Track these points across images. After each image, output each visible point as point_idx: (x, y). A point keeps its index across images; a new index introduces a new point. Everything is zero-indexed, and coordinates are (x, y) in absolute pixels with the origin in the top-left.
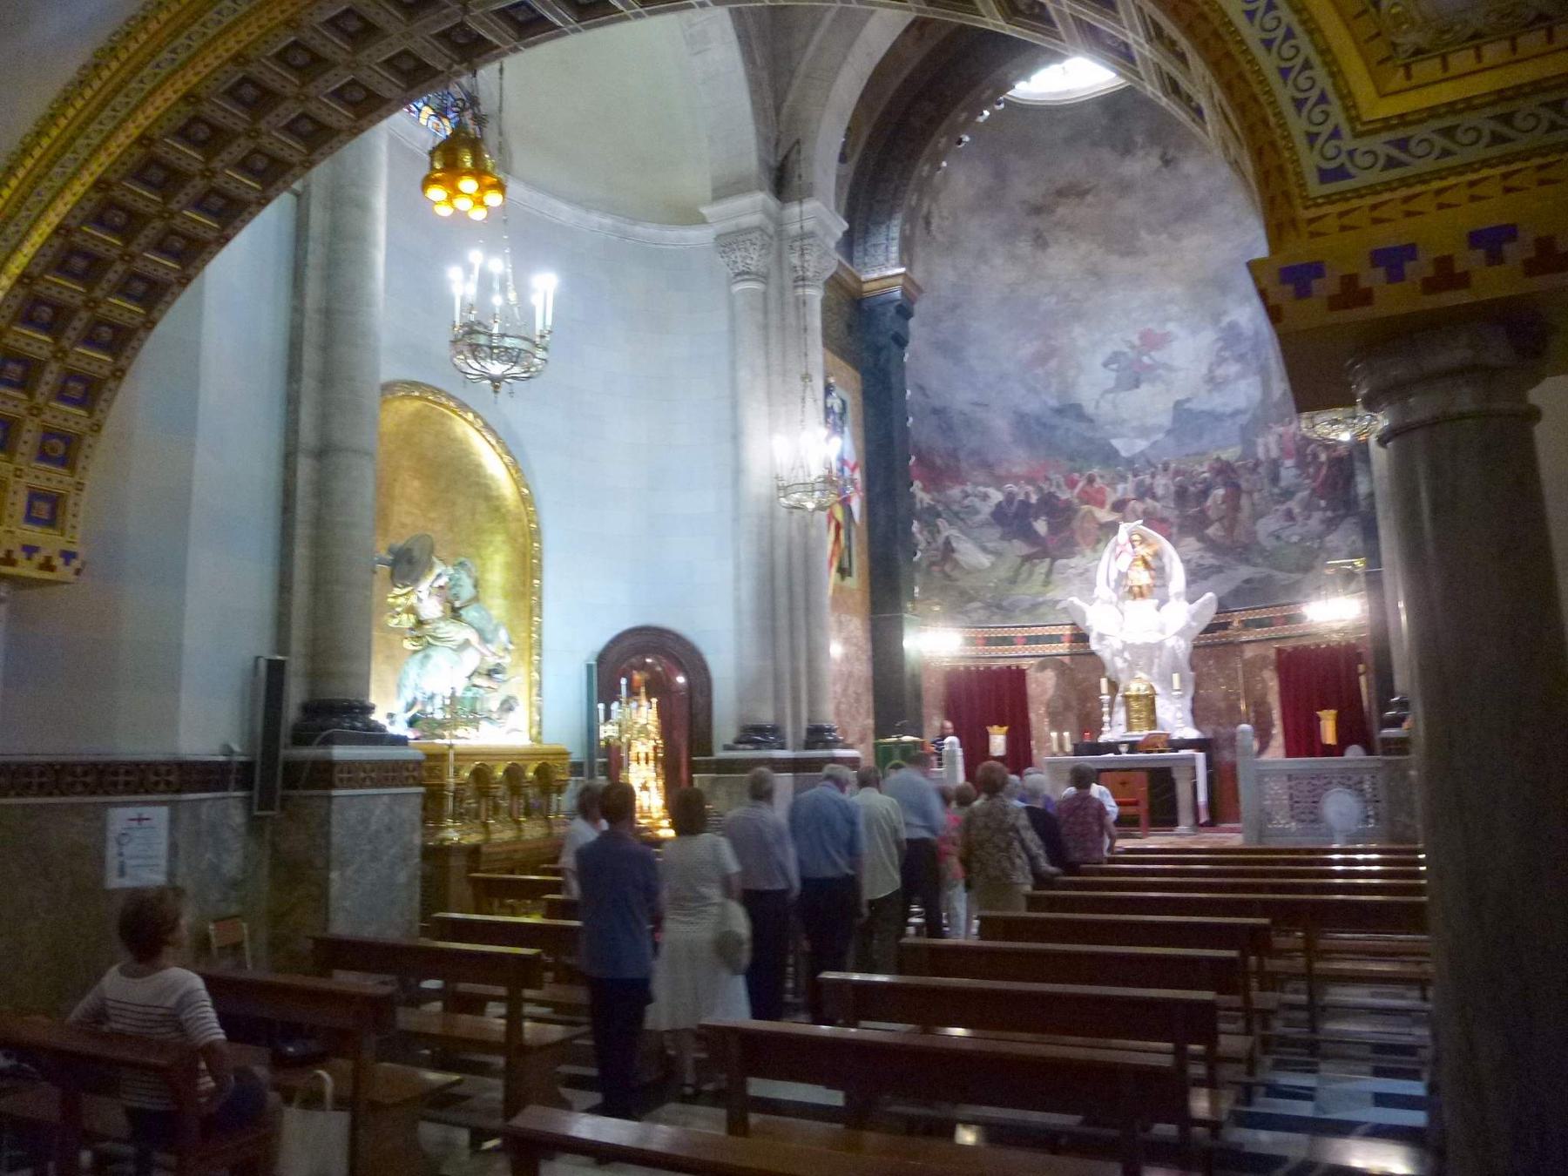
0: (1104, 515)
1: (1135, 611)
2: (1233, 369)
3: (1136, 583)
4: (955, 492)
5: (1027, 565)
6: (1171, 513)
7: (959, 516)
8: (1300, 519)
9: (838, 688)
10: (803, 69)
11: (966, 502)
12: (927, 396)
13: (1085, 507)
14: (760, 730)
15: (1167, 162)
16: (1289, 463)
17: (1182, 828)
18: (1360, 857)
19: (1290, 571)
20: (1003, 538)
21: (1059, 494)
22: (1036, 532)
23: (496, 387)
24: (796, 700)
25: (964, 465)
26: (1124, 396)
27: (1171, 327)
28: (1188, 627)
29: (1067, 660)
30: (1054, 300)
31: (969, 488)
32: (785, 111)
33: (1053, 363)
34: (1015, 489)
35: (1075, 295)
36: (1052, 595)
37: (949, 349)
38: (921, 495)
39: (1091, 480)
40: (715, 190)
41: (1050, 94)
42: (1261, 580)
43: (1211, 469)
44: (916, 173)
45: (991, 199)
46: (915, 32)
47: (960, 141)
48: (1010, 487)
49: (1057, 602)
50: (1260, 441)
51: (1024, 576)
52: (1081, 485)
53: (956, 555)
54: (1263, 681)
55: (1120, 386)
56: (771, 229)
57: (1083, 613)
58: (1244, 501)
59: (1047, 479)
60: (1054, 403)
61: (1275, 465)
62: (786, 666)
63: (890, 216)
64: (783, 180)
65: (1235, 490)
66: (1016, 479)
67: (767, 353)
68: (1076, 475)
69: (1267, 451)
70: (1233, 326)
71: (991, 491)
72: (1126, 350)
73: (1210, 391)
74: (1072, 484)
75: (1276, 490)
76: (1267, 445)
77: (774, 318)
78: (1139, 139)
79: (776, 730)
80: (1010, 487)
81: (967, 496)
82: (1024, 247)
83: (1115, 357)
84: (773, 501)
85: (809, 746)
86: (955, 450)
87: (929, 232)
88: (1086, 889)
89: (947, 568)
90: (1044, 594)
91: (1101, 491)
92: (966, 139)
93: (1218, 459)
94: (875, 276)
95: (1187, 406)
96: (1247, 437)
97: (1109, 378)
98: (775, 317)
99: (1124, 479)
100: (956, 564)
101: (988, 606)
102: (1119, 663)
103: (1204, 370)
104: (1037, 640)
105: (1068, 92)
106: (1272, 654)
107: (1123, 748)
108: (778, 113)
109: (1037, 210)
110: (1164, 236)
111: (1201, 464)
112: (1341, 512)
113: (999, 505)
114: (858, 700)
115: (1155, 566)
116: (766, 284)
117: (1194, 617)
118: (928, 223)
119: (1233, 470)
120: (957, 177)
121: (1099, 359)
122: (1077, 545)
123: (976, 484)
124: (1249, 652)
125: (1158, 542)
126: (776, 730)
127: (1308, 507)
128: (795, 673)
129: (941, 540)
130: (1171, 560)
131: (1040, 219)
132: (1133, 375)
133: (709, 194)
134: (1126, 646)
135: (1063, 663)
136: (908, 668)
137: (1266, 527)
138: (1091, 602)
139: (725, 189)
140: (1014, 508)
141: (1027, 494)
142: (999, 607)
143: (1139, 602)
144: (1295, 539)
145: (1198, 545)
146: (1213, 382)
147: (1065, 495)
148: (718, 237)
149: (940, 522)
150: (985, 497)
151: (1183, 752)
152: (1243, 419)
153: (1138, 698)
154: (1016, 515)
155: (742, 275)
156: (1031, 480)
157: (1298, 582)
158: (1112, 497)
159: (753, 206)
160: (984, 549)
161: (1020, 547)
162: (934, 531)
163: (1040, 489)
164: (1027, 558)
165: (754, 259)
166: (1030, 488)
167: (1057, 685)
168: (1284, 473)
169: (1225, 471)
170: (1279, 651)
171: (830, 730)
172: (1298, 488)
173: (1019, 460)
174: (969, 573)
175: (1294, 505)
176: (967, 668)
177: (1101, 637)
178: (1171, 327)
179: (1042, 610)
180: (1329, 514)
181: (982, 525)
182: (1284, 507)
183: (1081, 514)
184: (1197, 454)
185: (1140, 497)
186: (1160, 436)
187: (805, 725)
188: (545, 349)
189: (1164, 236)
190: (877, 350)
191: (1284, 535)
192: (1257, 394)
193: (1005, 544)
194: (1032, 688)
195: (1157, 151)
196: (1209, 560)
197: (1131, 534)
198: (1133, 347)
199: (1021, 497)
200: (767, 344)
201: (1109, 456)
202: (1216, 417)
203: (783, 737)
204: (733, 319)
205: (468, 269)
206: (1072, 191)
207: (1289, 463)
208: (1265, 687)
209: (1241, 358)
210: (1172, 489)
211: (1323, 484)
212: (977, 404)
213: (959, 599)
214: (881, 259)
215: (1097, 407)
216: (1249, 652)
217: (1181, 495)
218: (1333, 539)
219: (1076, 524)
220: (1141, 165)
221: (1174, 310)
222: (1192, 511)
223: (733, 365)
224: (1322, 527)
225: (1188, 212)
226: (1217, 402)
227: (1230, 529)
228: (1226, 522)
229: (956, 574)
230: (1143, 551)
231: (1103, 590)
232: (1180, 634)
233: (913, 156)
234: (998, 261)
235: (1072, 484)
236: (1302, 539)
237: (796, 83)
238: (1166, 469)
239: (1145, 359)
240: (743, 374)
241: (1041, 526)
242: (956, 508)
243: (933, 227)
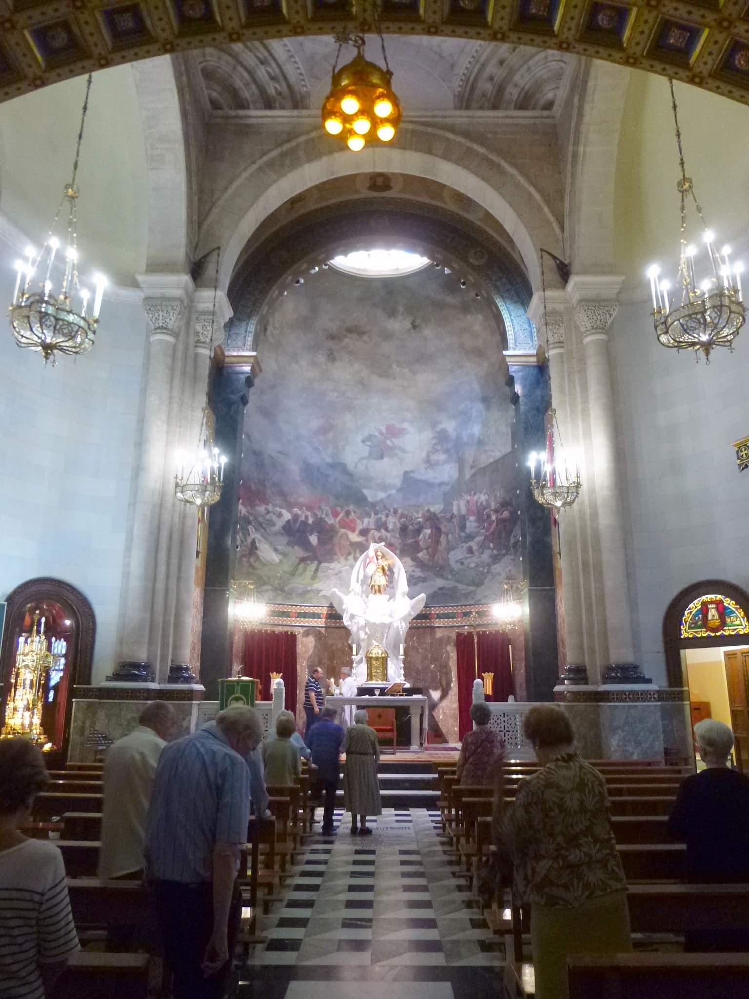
0: (354, 537)
1: (375, 601)
2: (442, 457)
3: (378, 583)
4: (261, 509)
5: (302, 565)
6: (397, 541)
7: (263, 526)
8: (477, 554)
10: (221, 203)
11: (268, 517)
12: (251, 442)
13: (343, 530)
14: (136, 666)
15: (414, 327)
16: (472, 518)
17: (415, 747)
18: (519, 768)
19: (468, 585)
20: (288, 544)
21: (327, 520)
22: (309, 543)
23: (47, 354)
24: (165, 645)
25: (269, 492)
26: (375, 462)
27: (405, 425)
28: (410, 615)
29: (323, 630)
30: (336, 394)
31: (270, 508)
32: (205, 226)
33: (330, 435)
34: (299, 512)
35: (349, 394)
36: (317, 586)
37: (267, 413)
38: (242, 509)
39: (348, 513)
40: (148, 265)
41: (358, 270)
42: (449, 589)
43: (423, 516)
44: (269, 296)
45: (305, 323)
46: (289, 204)
47: (298, 282)
48: (296, 510)
49: (319, 591)
50: (455, 503)
51: (300, 571)
52: (341, 516)
53: (258, 552)
54: (447, 652)
55: (370, 456)
56: (186, 303)
57: (341, 602)
58: (443, 539)
59: (320, 508)
60: (329, 460)
61: (463, 519)
62: (159, 619)
63: (249, 317)
64: (197, 271)
65: (437, 531)
66: (301, 506)
67: (171, 388)
68: (339, 509)
69: (459, 509)
70: (444, 432)
71: (284, 512)
72: (377, 434)
73: (426, 468)
74: (335, 514)
75: (463, 534)
76: (459, 506)
77: (179, 365)
78: (401, 309)
80: (296, 510)
81: (268, 512)
82: (321, 358)
83: (370, 437)
84: (163, 494)
85: (171, 680)
86: (264, 481)
87: (265, 335)
88: (659, 794)
89: (252, 560)
90: (311, 585)
91: (353, 521)
92: (302, 281)
93: (428, 511)
94: (235, 354)
95: (412, 475)
96: (447, 498)
97: (365, 450)
98: (181, 363)
99: (369, 516)
100: (258, 558)
101: (275, 589)
102: (362, 635)
103: (424, 455)
104: (305, 615)
105: (364, 270)
106: (454, 636)
107: (377, 692)
108: (200, 225)
109: (332, 337)
110: (407, 370)
111: (417, 512)
112: (504, 552)
113: (288, 522)
115: (388, 572)
116: (177, 340)
117: (413, 608)
119: (438, 519)
120: (288, 304)
121: (359, 438)
122: (336, 554)
123: (275, 506)
124: (439, 634)
125: (392, 558)
126: (147, 667)
127: (482, 547)
128: (166, 623)
129: (249, 540)
130: (399, 570)
131: (333, 343)
132: (380, 451)
133: (144, 268)
134: (367, 623)
135: (320, 632)
136: (229, 627)
137: (456, 555)
138: (347, 592)
139: (155, 267)
140: (297, 525)
141: (307, 517)
142: (282, 590)
143: (378, 596)
144: (473, 565)
145: (412, 563)
146: (429, 463)
147: (330, 521)
148: (147, 299)
149: (250, 527)
150: (280, 515)
151: (415, 696)
152: (446, 488)
153: (377, 659)
154: (298, 530)
155: (163, 329)
156: (309, 508)
157: (472, 592)
158: (360, 526)
159: (178, 282)
160: (276, 550)
161: (299, 552)
162: (246, 533)
163: (315, 515)
164: (303, 560)
165: (173, 320)
166: (309, 513)
167: (315, 647)
168: (468, 524)
169: (432, 519)
170: (459, 635)
171: (187, 669)
172: (477, 534)
173: (304, 494)
174: (265, 565)
175: (474, 545)
176: (260, 631)
177: (352, 617)
178: (405, 425)
179: (308, 596)
180: (495, 552)
181: (276, 534)
182: (468, 545)
183: (340, 534)
184: (415, 506)
185: (378, 529)
186: (393, 492)
188: (94, 332)
189: (407, 370)
190: (230, 404)
191: (466, 562)
192: (456, 475)
193: (290, 548)
194: (300, 648)
195: (411, 319)
196: (418, 573)
197: (376, 552)
198: (381, 433)
199: (303, 518)
200: (172, 382)
201: (360, 500)
202: (430, 485)
203: (153, 673)
204: (148, 356)
205: (26, 259)
206: (355, 330)
207: (472, 518)
208: (448, 657)
209: (447, 451)
210: (398, 525)
211: (493, 533)
212: (280, 452)
213: (262, 584)
214: (240, 344)
215: (356, 467)
216: (439, 634)
217: (404, 529)
218: (497, 568)
219: (336, 540)
220: (399, 325)
221: (409, 415)
222: (410, 541)
223: (144, 391)
224: (489, 560)
226: (430, 475)
227: (432, 556)
228: (430, 550)
229: (257, 565)
230: (384, 563)
231: (356, 586)
232: (404, 619)
233: (271, 281)
234: (303, 363)
235: (335, 514)
236: (477, 566)
237: (215, 211)
238: (395, 512)
239: (388, 442)
240: (153, 400)
241: (314, 539)
242: (261, 519)
243: (268, 332)
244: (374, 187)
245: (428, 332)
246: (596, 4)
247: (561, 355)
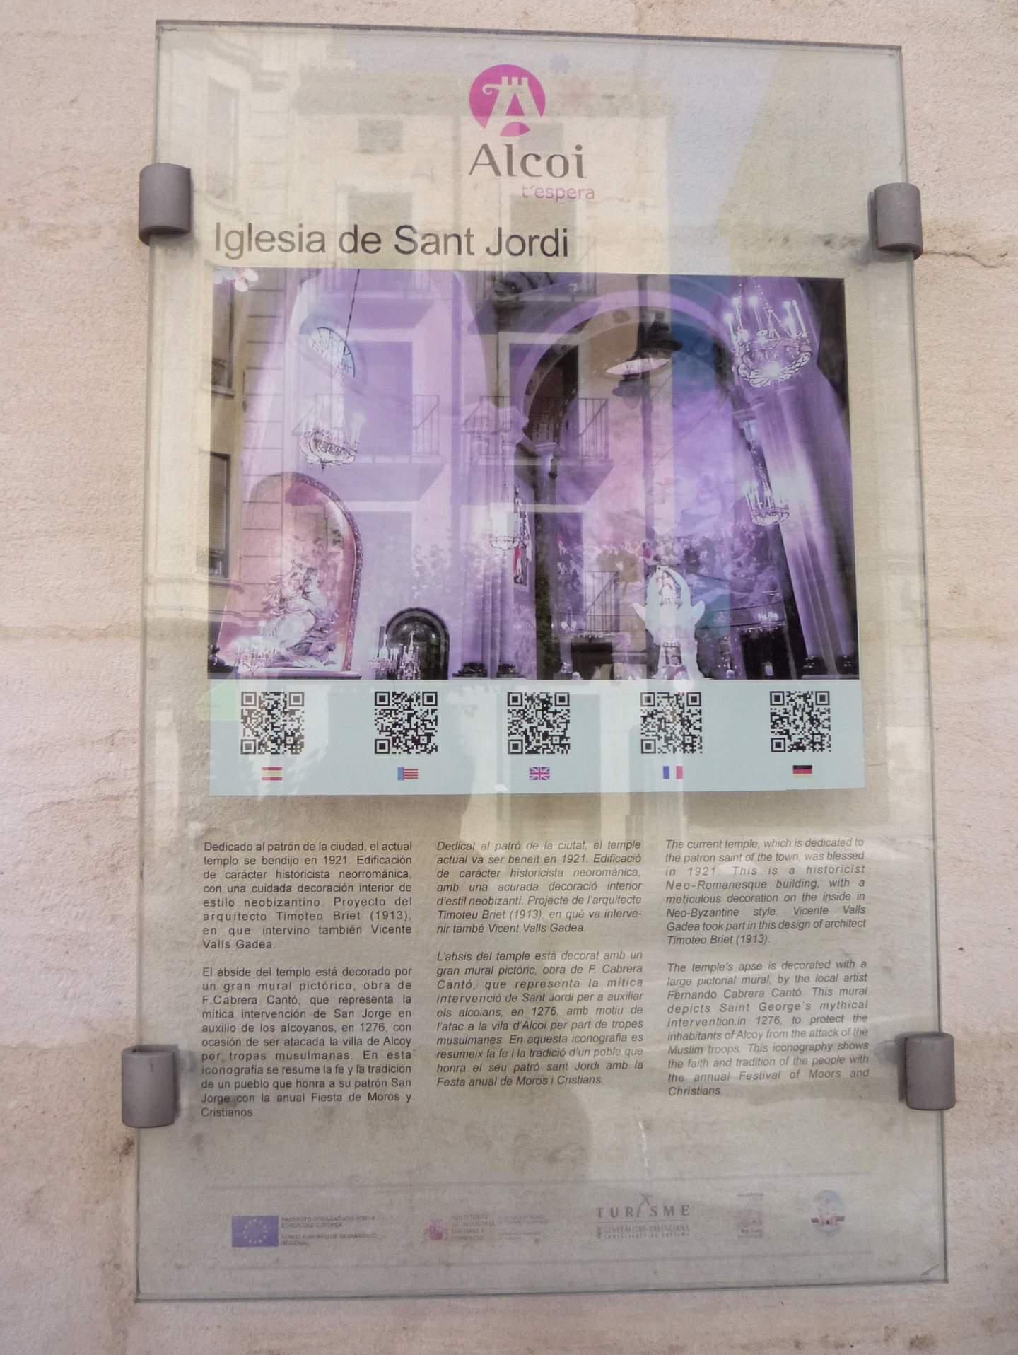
9: (517, 643)
64: (497, 399)
79: (482, 666)
114: (528, 650)
118: (567, 425)
127: (748, 562)
128: (493, 634)
146: (699, 502)
150: (593, 551)
162: (568, 566)
172: (743, 551)
175: (741, 559)
187: (498, 663)
196: (702, 585)
225: (503, 499)
244: (618, 320)
245: (684, 409)
246: (899, 48)
247: (762, 408)
